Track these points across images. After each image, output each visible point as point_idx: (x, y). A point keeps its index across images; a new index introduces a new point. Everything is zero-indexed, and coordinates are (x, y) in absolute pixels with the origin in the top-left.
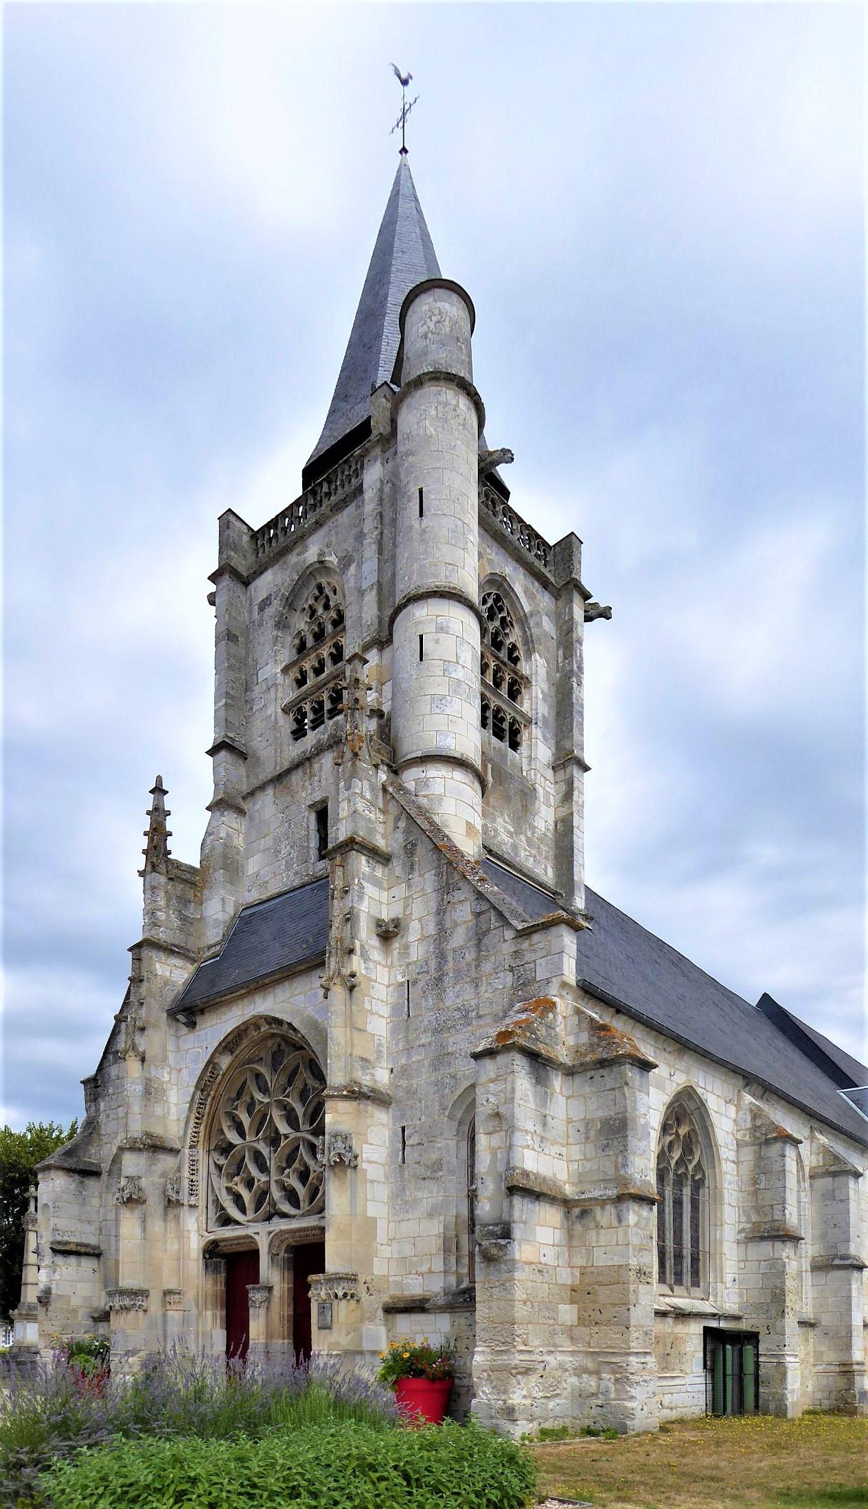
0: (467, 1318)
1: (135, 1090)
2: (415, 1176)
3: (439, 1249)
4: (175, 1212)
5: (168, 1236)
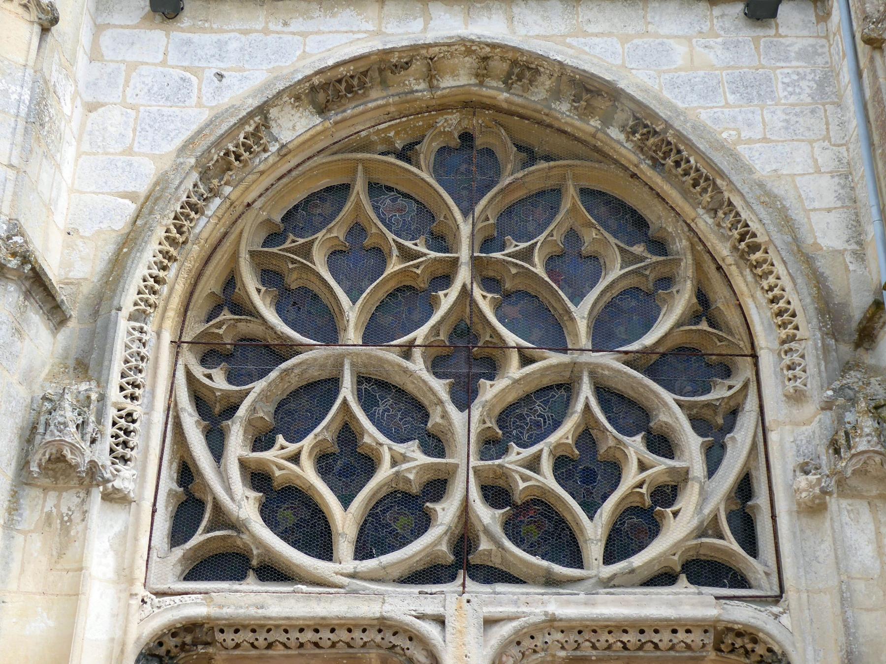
4: (70, 500)
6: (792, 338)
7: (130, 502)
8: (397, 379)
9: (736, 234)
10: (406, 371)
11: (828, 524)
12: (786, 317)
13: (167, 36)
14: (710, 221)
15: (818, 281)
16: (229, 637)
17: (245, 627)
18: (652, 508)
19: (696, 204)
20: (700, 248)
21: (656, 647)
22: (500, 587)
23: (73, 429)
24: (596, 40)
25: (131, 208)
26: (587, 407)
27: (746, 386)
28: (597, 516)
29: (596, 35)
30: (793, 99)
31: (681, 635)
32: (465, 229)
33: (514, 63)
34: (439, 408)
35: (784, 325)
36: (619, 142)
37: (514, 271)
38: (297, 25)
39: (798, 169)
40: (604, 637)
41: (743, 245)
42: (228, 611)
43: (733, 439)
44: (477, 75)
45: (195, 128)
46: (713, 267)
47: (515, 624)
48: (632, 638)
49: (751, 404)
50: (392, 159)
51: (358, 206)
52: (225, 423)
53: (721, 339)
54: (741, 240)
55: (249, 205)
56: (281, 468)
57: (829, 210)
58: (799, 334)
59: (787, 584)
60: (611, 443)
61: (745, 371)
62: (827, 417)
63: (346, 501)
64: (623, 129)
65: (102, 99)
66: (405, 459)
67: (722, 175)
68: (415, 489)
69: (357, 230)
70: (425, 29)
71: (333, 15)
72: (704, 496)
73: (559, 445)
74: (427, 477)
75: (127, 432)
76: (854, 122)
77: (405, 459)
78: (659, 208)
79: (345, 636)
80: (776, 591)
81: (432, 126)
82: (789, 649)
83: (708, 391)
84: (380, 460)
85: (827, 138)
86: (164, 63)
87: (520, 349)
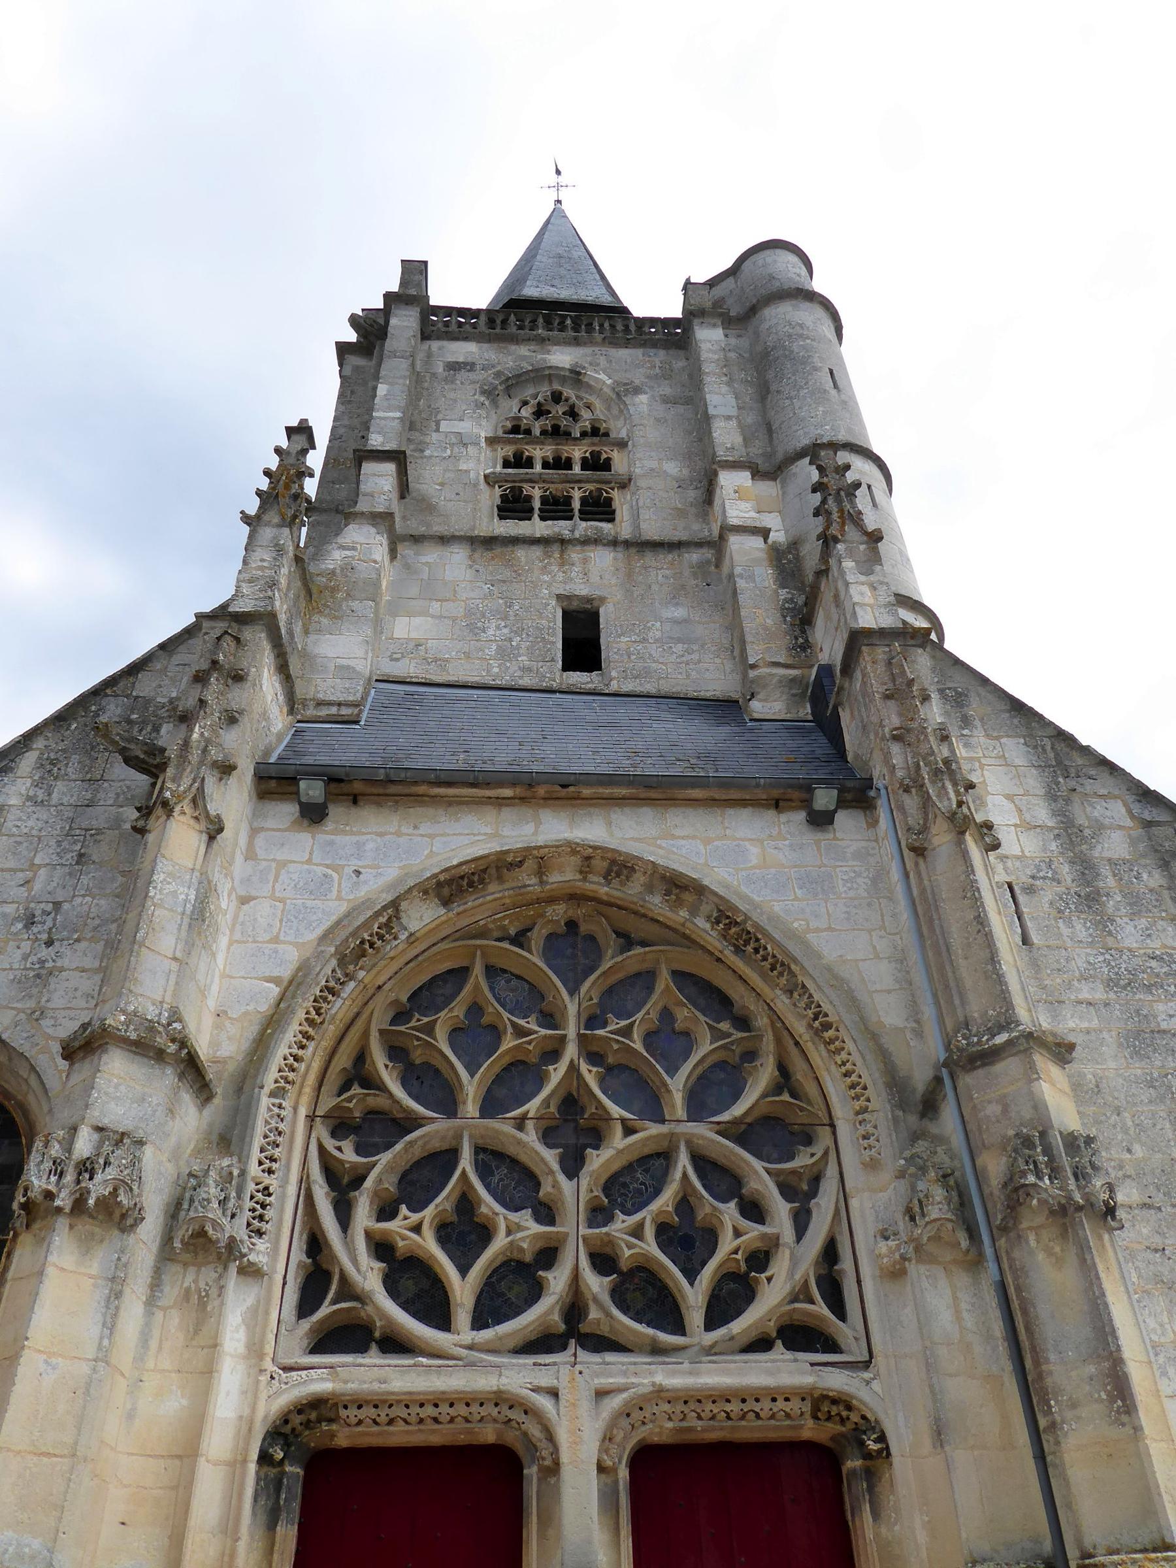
1: (174, 894)
4: (209, 1274)
5: (150, 1364)
6: (865, 1110)
8: (512, 1150)
9: (810, 1013)
10: (519, 1142)
12: (858, 1090)
13: (313, 838)
14: (787, 1001)
15: (884, 1055)
16: (352, 1413)
17: (367, 1402)
18: (747, 1274)
20: (779, 1025)
21: (758, 1416)
22: (610, 1357)
24: (683, 842)
25: (275, 991)
26: (685, 1175)
27: (826, 1153)
29: (683, 838)
30: (851, 894)
31: (780, 1404)
32: (572, 1009)
33: (613, 862)
34: (550, 1179)
35: (857, 1097)
37: (616, 1047)
38: (425, 828)
42: (352, 1386)
43: (818, 1204)
44: (581, 872)
45: (334, 918)
46: (791, 1042)
48: (734, 1407)
49: (831, 1171)
50: (506, 945)
51: (477, 987)
52: (352, 1194)
53: (802, 1109)
54: (816, 1018)
55: (379, 987)
56: (404, 1238)
57: (889, 992)
58: (871, 1106)
59: (876, 1349)
60: (708, 1210)
61: (824, 1138)
62: (902, 1185)
63: (464, 1270)
64: (708, 918)
65: (254, 893)
66: (520, 1228)
67: (795, 961)
68: (528, 1258)
69: (475, 1010)
71: (457, 820)
72: (794, 1262)
73: (661, 1212)
75: (263, 1206)
76: (905, 916)
78: (741, 988)
81: (542, 915)
82: (882, 1417)
83: (791, 1158)
85: (883, 927)
86: (309, 861)
87: (623, 1121)
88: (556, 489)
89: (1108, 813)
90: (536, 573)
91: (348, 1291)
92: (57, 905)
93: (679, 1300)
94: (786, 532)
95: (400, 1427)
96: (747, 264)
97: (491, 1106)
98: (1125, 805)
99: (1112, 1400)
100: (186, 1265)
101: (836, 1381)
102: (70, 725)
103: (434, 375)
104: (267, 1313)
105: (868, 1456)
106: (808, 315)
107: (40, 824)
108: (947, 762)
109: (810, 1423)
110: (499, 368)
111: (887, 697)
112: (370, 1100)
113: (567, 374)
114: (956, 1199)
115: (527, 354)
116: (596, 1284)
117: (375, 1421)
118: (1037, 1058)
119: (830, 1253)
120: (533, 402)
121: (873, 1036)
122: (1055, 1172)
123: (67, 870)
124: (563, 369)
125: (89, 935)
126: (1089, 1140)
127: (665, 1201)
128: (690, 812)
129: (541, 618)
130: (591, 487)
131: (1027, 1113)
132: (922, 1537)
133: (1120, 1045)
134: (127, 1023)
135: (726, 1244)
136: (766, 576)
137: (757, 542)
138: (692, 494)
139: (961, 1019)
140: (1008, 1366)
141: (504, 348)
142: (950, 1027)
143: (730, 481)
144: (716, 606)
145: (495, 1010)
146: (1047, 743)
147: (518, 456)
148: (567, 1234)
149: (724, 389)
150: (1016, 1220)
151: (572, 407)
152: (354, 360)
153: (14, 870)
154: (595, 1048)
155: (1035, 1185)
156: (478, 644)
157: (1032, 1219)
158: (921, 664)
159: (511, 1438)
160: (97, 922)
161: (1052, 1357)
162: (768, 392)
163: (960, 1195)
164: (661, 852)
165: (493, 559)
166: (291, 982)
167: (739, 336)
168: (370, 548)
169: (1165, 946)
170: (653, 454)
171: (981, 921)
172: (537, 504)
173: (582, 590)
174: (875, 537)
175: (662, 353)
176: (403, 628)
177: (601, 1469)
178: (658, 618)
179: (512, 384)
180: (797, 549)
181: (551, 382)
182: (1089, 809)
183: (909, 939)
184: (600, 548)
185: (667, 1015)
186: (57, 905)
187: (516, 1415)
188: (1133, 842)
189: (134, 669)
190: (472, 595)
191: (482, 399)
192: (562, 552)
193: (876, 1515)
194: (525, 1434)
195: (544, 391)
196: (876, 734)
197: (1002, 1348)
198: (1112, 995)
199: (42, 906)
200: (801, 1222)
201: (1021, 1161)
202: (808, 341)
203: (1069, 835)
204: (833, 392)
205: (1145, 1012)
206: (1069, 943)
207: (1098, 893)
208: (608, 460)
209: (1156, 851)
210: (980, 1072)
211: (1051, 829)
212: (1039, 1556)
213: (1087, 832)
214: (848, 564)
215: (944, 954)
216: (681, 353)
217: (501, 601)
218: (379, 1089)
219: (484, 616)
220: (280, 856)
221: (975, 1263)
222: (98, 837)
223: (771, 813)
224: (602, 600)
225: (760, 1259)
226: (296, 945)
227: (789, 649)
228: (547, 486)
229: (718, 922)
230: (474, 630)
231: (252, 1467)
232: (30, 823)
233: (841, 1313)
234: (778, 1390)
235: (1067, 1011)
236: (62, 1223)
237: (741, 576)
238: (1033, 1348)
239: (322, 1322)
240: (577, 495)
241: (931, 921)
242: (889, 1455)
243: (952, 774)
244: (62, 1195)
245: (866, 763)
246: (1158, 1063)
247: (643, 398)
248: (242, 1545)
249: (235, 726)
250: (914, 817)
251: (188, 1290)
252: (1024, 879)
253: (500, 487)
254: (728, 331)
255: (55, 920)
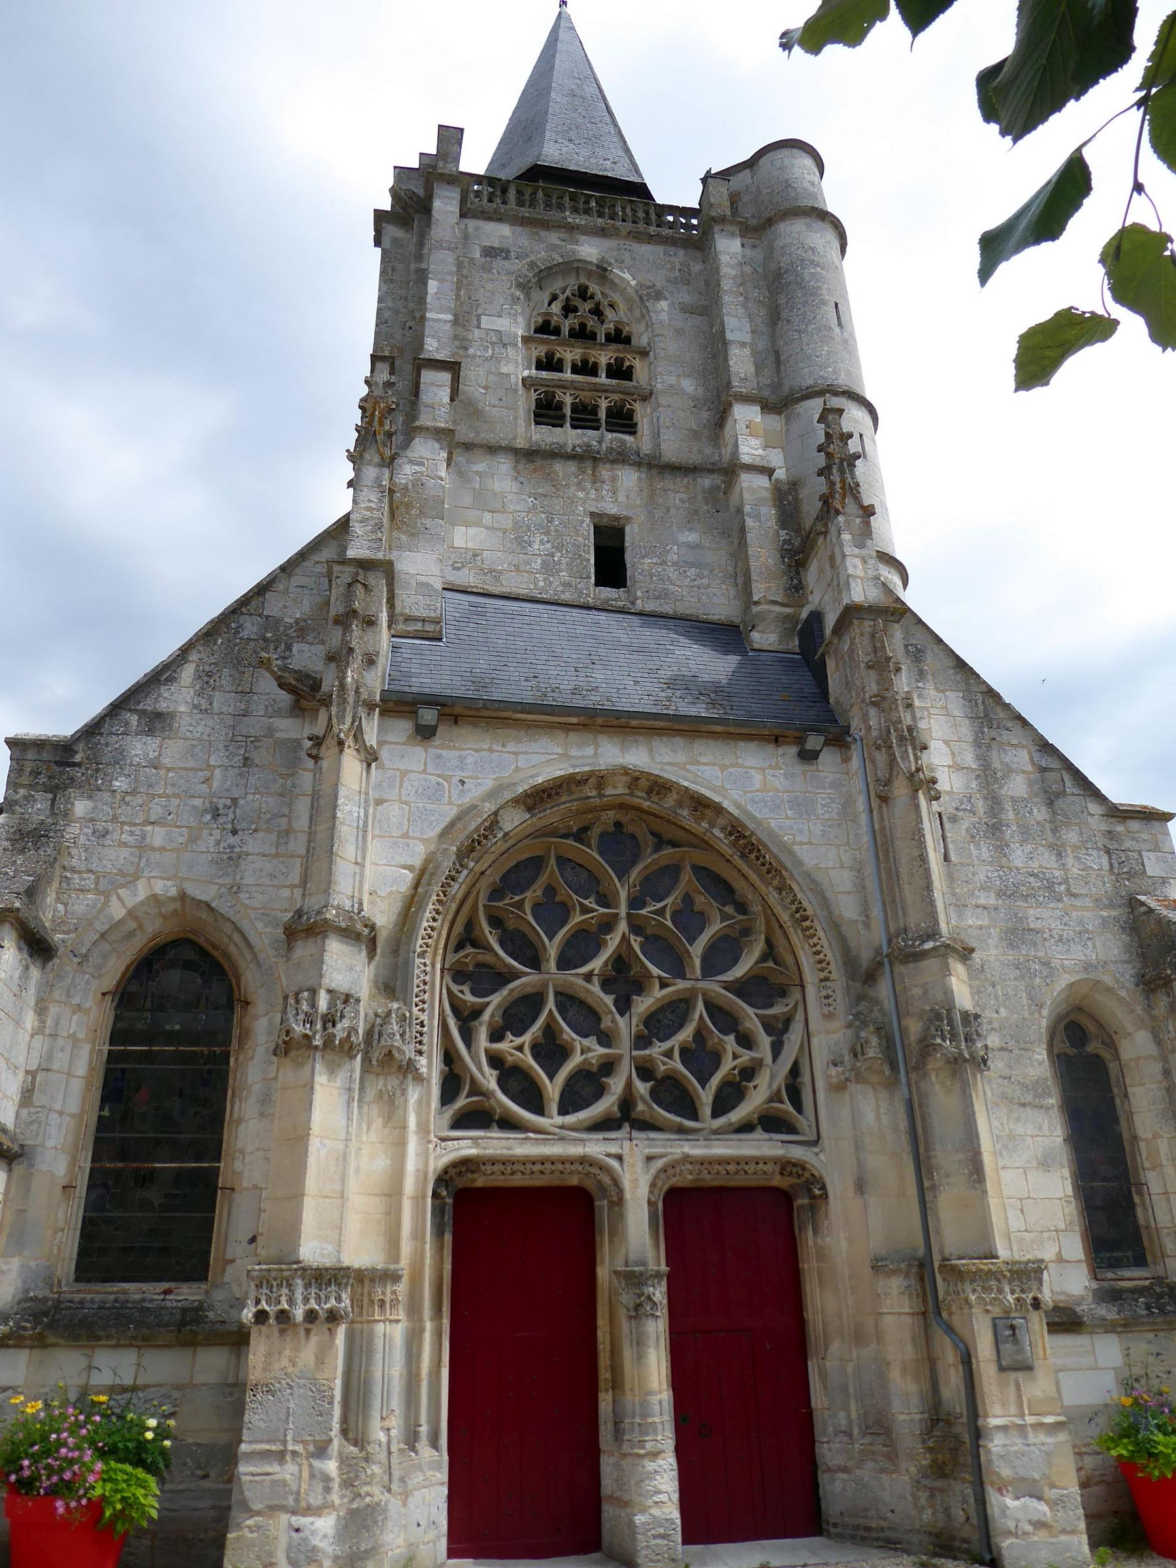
0: (1150, 1342)
2: (1004, 1096)
3: (1071, 1223)
4: (393, 1082)
6: (826, 979)
7: (423, 1080)
8: (582, 995)
9: (794, 907)
10: (588, 991)
11: (847, 1097)
12: (824, 965)
13: (426, 751)
14: (777, 896)
15: (843, 940)
16: (488, 1168)
17: (498, 1161)
18: (740, 1083)
19: (768, 884)
20: (769, 912)
21: (746, 1173)
22: (653, 1135)
23: (398, 1037)
24: (706, 768)
25: (409, 876)
26: (701, 1016)
27: (796, 1004)
28: (707, 1087)
29: (705, 764)
30: (827, 816)
31: (761, 1166)
32: (623, 895)
33: (655, 783)
34: (610, 1017)
35: (822, 970)
36: (720, 839)
37: (653, 923)
38: (511, 747)
39: (830, 865)
40: (717, 1167)
41: (798, 915)
42: (489, 1152)
43: (789, 1039)
44: (629, 788)
45: (448, 820)
46: (777, 925)
47: (665, 1160)
48: (732, 1168)
49: (799, 1016)
50: (570, 842)
51: (552, 874)
52: (472, 1023)
53: (781, 973)
54: (797, 912)
55: (483, 873)
56: (511, 1055)
57: (849, 893)
58: (832, 977)
59: (822, 1134)
60: (716, 1040)
61: (796, 994)
62: (850, 1033)
63: (551, 1077)
64: (723, 829)
65: (385, 797)
66: (589, 1050)
67: (786, 869)
68: (595, 1069)
69: (550, 890)
70: (596, 755)
71: (535, 741)
72: (773, 1077)
73: (684, 1041)
74: (602, 1061)
75: (421, 1035)
76: (866, 839)
77: (589, 1050)
78: (743, 883)
79: (560, 1167)
80: (815, 1138)
81: (599, 819)
82: (824, 1174)
83: (771, 1006)
84: (573, 1050)
85: (848, 844)
86: (424, 771)
87: (660, 978)
88: (585, 396)
89: (1016, 759)
90: (573, 489)
91: (476, 1089)
92: (235, 801)
93: (695, 1099)
94: (787, 470)
95: (519, 1176)
96: (764, 161)
97: (565, 963)
98: (1030, 754)
99: (971, 1175)
100: (377, 1075)
101: (797, 1153)
102: (216, 641)
103: (472, 260)
104: (429, 1105)
105: (814, 1197)
106: (822, 238)
107: (208, 730)
108: (910, 729)
109: (778, 1177)
110: (532, 258)
111: (869, 667)
112: (480, 956)
113: (594, 268)
114: (885, 1044)
115: (558, 242)
116: (642, 1088)
117: (503, 1173)
118: (951, 961)
119: (795, 1071)
120: (562, 297)
121: (835, 925)
122: (954, 1037)
123: (236, 771)
124: (591, 263)
125: (264, 827)
126: (977, 1016)
127: (686, 1034)
128: (711, 742)
129: (578, 535)
130: (616, 397)
131: (939, 996)
132: (844, 1245)
133: (1001, 938)
134: (337, 915)
135: (727, 1065)
136: (769, 513)
137: (762, 482)
138: (705, 415)
139: (902, 926)
140: (907, 1148)
141: (537, 233)
142: (892, 929)
143: (745, 415)
144: (724, 533)
145: (565, 893)
146: (979, 697)
147: (550, 355)
148: (620, 1057)
149: (741, 310)
150: (924, 1064)
151: (598, 304)
152: (392, 231)
153: (196, 770)
154: (638, 923)
155: (940, 1045)
156: (526, 557)
157: (935, 1063)
158: (896, 640)
159: (589, 1184)
160: (268, 816)
161: (938, 1147)
162: (779, 318)
163: (887, 1041)
164: (689, 775)
165: (534, 471)
166: (423, 871)
167: (754, 246)
168: (436, 464)
169: (1041, 867)
170: (672, 369)
171: (923, 859)
172: (568, 411)
173: (612, 509)
174: (869, 511)
175: (681, 252)
176: (463, 537)
177: (649, 1203)
178: (675, 542)
179: (544, 275)
180: (796, 491)
181: (578, 274)
182: (1003, 755)
183: (867, 855)
184: (626, 467)
185: (687, 899)
186: (235, 801)
187: (593, 1170)
188: (1030, 784)
189: (262, 589)
190: (518, 508)
191: (518, 293)
192: (594, 469)
193: (815, 1232)
194: (599, 1182)
195: (572, 284)
196: (858, 695)
197: (904, 1137)
198: (1000, 902)
199: (223, 800)
200: (777, 1049)
201: (933, 1028)
202: (818, 269)
203: (986, 776)
204: (837, 330)
205: (1020, 915)
206: (976, 862)
207: (1001, 824)
208: (631, 367)
209: (1046, 792)
210: (911, 965)
211: (974, 770)
212: (915, 1258)
213: (999, 774)
214: (846, 537)
215: (895, 879)
216: (699, 254)
217: (543, 516)
218: (485, 948)
219: (529, 530)
220: (403, 765)
221: (891, 1084)
222: (257, 744)
223: (772, 747)
224: (628, 519)
225: (749, 1073)
226: (423, 841)
227: (786, 589)
228: (578, 393)
229: (730, 834)
230: (522, 543)
231: (429, 1200)
232: (200, 729)
233: (799, 1109)
234: (761, 1158)
235: (968, 912)
236: (318, 1055)
237: (749, 515)
238: (926, 1141)
239: (460, 1109)
240: (604, 405)
241: (887, 852)
242: (827, 1197)
243: (913, 739)
244: (317, 1037)
245: (846, 712)
246: (1024, 952)
247: (664, 304)
248: (428, 1246)
249: (373, 667)
250: (882, 773)
251: (381, 1091)
252: (951, 810)
253: (535, 391)
254: (745, 240)
255: (235, 813)
